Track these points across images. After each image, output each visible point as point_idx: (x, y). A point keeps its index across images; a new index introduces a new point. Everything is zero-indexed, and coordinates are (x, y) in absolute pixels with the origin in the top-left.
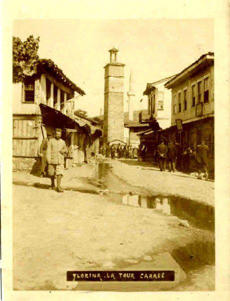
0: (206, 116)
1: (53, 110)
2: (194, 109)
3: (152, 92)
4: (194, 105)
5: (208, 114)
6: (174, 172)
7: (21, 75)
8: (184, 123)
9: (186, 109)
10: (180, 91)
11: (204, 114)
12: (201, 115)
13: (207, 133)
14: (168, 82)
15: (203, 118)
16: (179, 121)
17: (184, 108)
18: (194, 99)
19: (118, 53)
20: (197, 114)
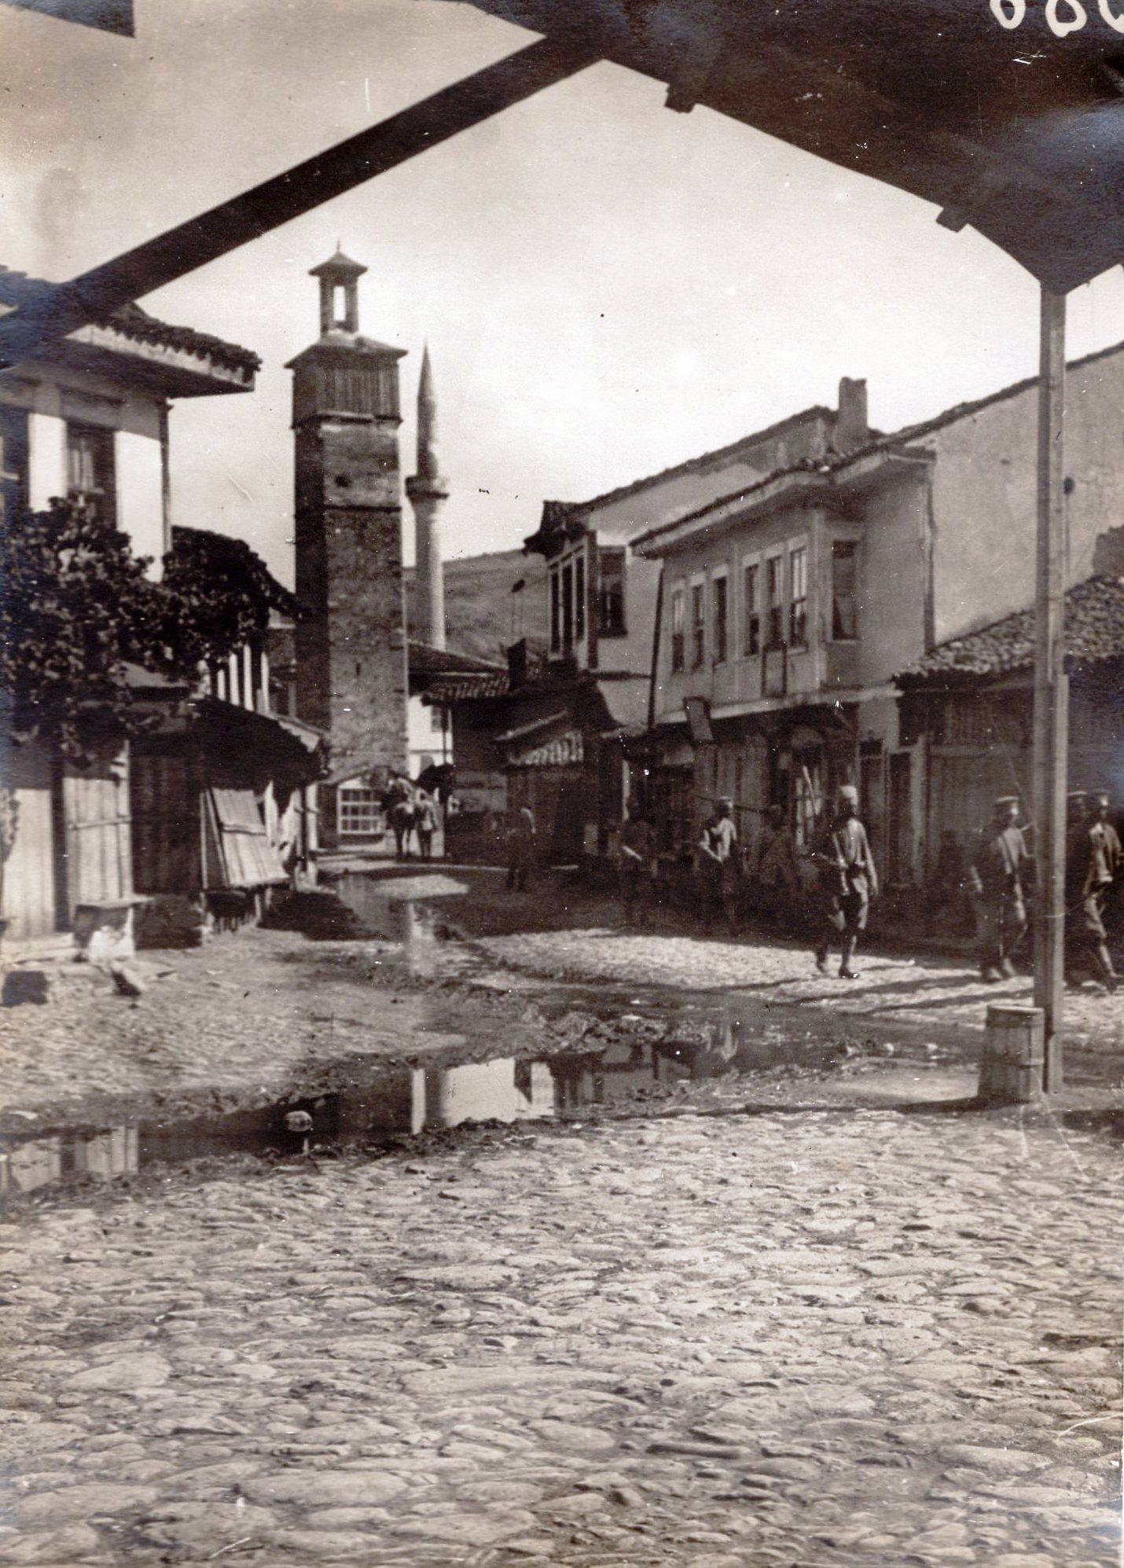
0: (799, 699)
1: (254, 718)
2: (754, 667)
3: (568, 547)
4: (753, 649)
5: (806, 694)
6: (502, 646)
7: (41, 525)
8: (718, 714)
9: (722, 658)
10: (698, 579)
11: (790, 690)
12: (780, 695)
13: (511, 71)
14: (650, 536)
15: (787, 703)
16: (697, 709)
17: (715, 652)
18: (754, 625)
19: (362, 282)
20: (768, 686)
